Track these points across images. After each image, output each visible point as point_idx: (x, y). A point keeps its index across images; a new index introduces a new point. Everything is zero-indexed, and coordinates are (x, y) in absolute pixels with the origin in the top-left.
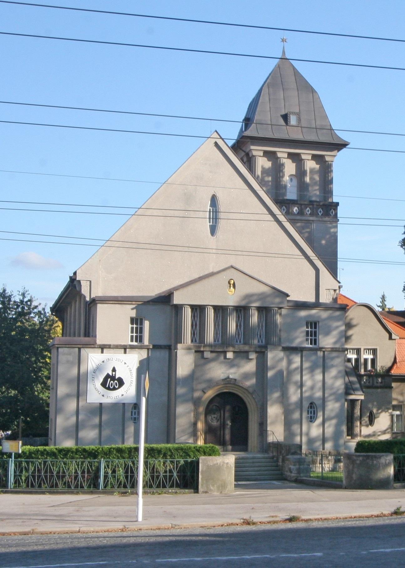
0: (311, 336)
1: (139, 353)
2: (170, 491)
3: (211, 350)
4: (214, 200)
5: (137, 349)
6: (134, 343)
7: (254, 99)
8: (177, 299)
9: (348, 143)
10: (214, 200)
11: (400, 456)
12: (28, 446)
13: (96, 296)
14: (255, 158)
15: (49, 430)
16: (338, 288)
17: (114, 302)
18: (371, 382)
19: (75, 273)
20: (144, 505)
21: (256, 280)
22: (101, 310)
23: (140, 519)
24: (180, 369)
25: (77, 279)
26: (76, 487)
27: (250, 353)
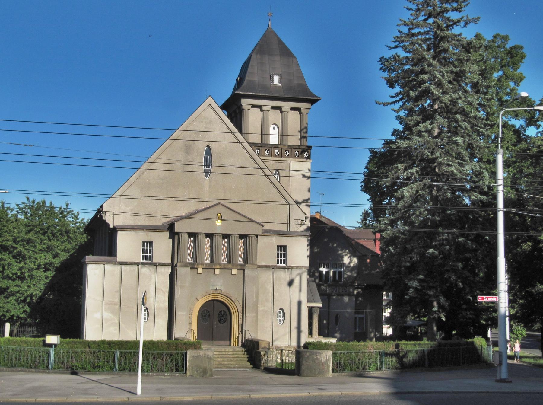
0: (281, 257)
1: (148, 269)
2: (166, 374)
3: (202, 267)
4: (209, 151)
5: (147, 266)
6: (145, 261)
7: (245, 62)
8: (178, 228)
9: (319, 99)
10: (209, 151)
11: (418, 348)
12: (64, 260)
13: (117, 225)
14: (244, 111)
15: (75, 340)
16: (304, 219)
17: (130, 230)
18: (338, 291)
19: (102, 206)
20: (143, 383)
21: (237, 214)
22: (121, 236)
23: (139, 392)
24: (179, 282)
25: (103, 210)
26: (35, 367)
27: (233, 270)
